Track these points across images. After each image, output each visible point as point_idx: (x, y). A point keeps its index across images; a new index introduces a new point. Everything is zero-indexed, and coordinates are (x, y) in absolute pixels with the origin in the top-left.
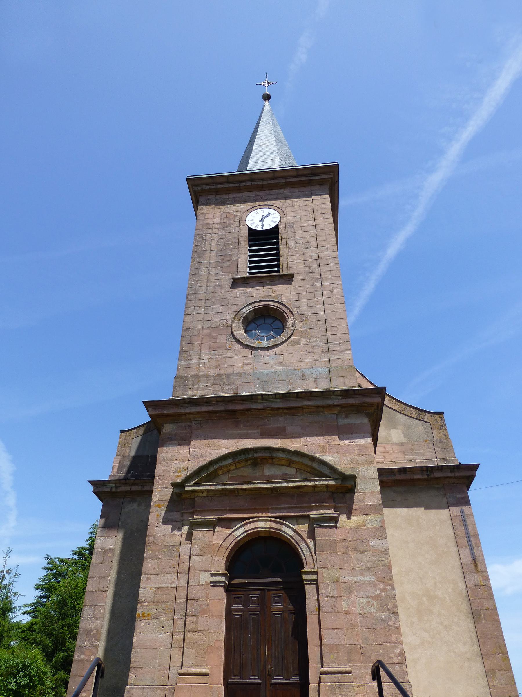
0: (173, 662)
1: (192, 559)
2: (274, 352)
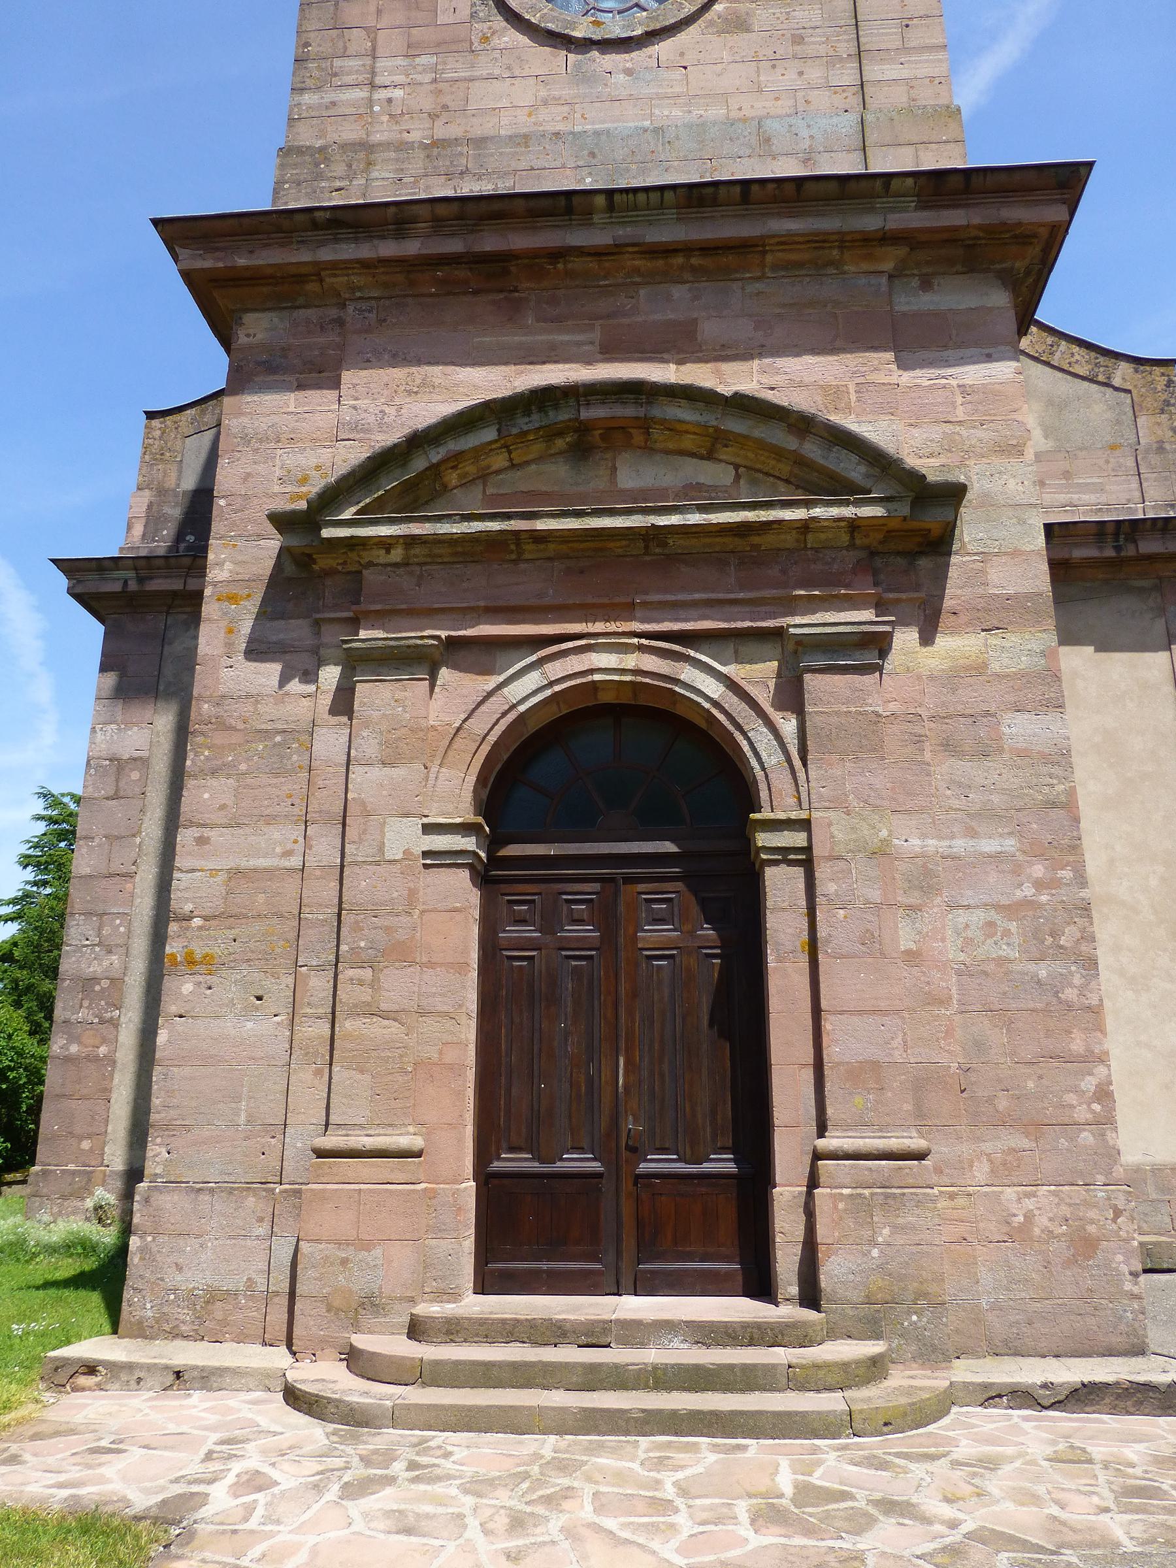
0: (296, 1111)
1: (353, 776)
2: (650, 57)
